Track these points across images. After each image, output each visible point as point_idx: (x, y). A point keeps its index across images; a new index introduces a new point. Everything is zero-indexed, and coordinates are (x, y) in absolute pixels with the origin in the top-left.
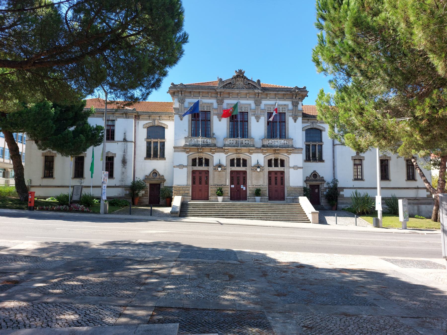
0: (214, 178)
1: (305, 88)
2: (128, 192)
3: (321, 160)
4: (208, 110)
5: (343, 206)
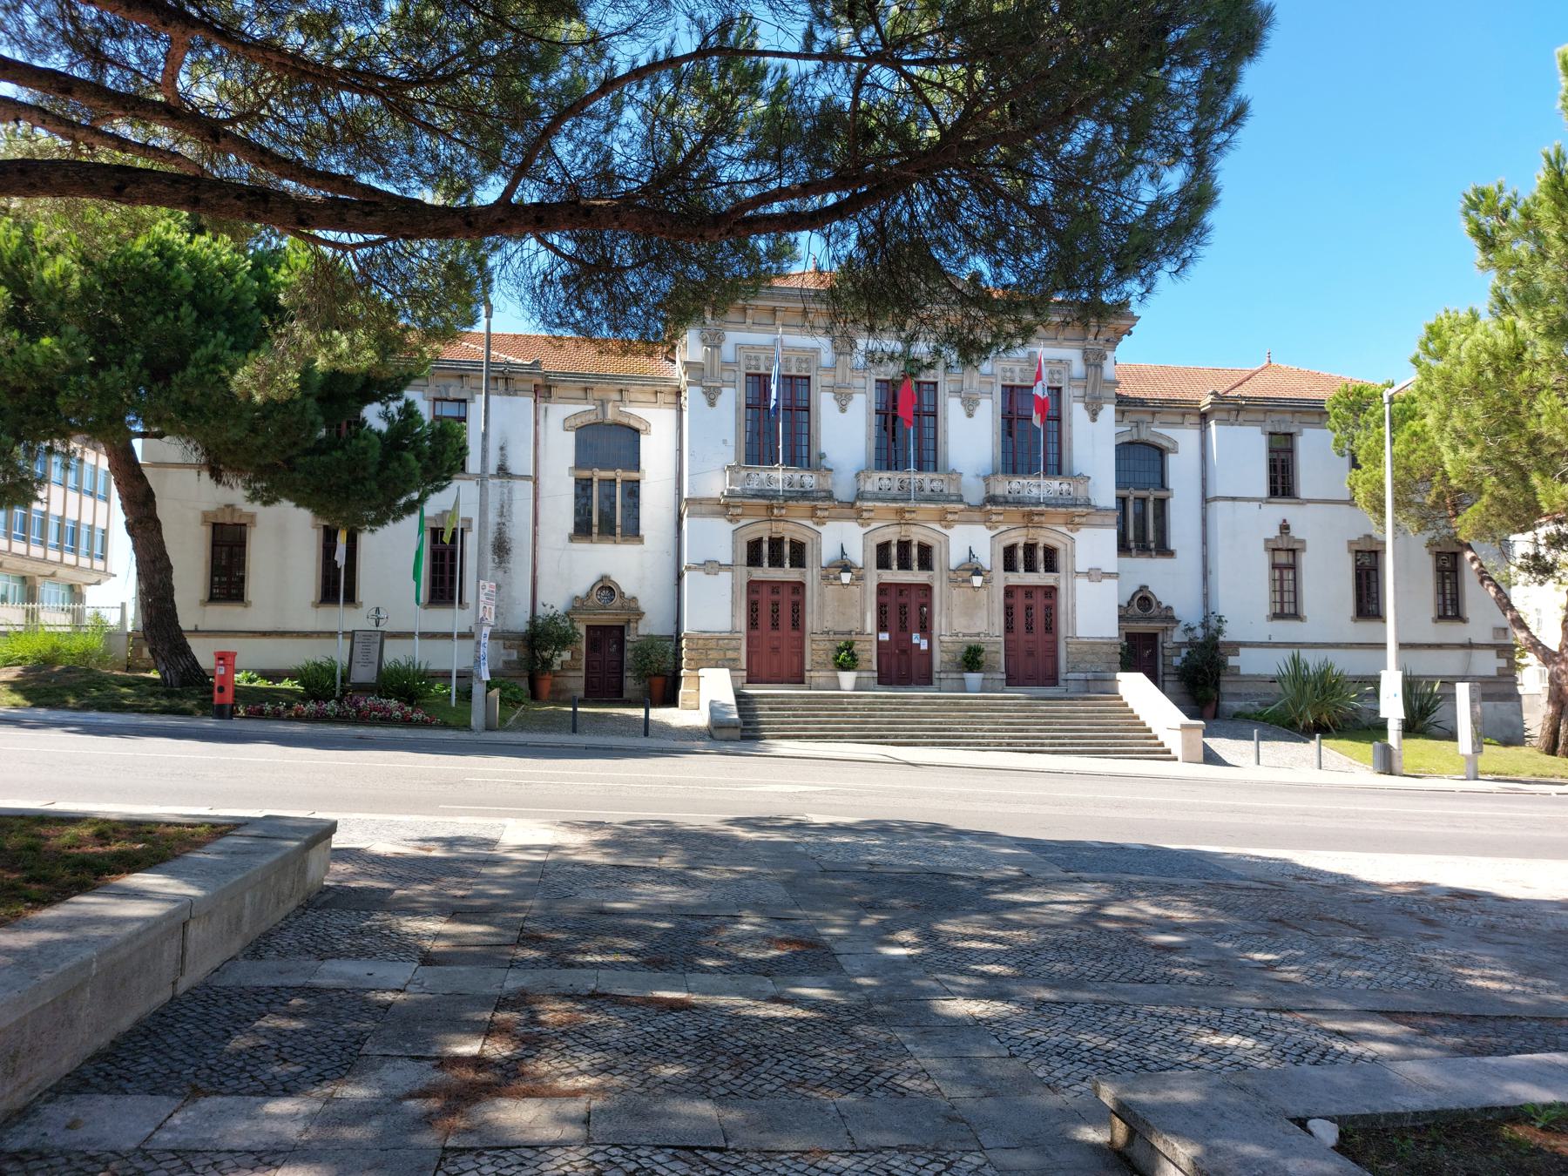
0: (822, 606)
2: (514, 655)
3: (1163, 550)
4: (804, 373)
5: (1237, 705)
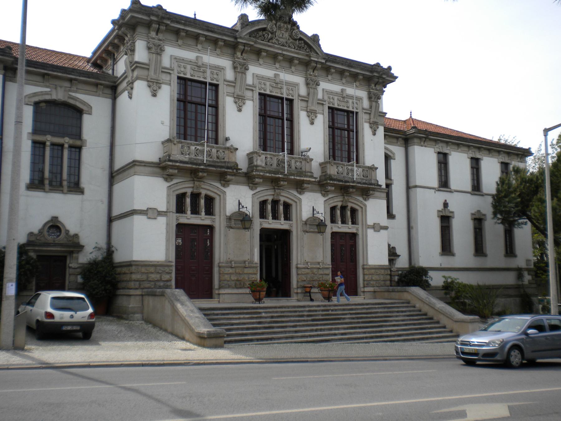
3: (76, 187)
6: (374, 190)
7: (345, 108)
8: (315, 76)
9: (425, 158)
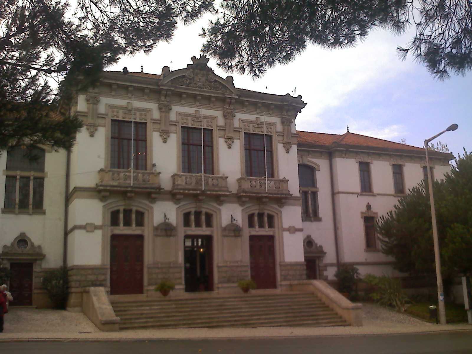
1: (300, 97)
4: (143, 121)
6: (286, 198)
7: (260, 133)
8: (232, 109)
9: (347, 170)
